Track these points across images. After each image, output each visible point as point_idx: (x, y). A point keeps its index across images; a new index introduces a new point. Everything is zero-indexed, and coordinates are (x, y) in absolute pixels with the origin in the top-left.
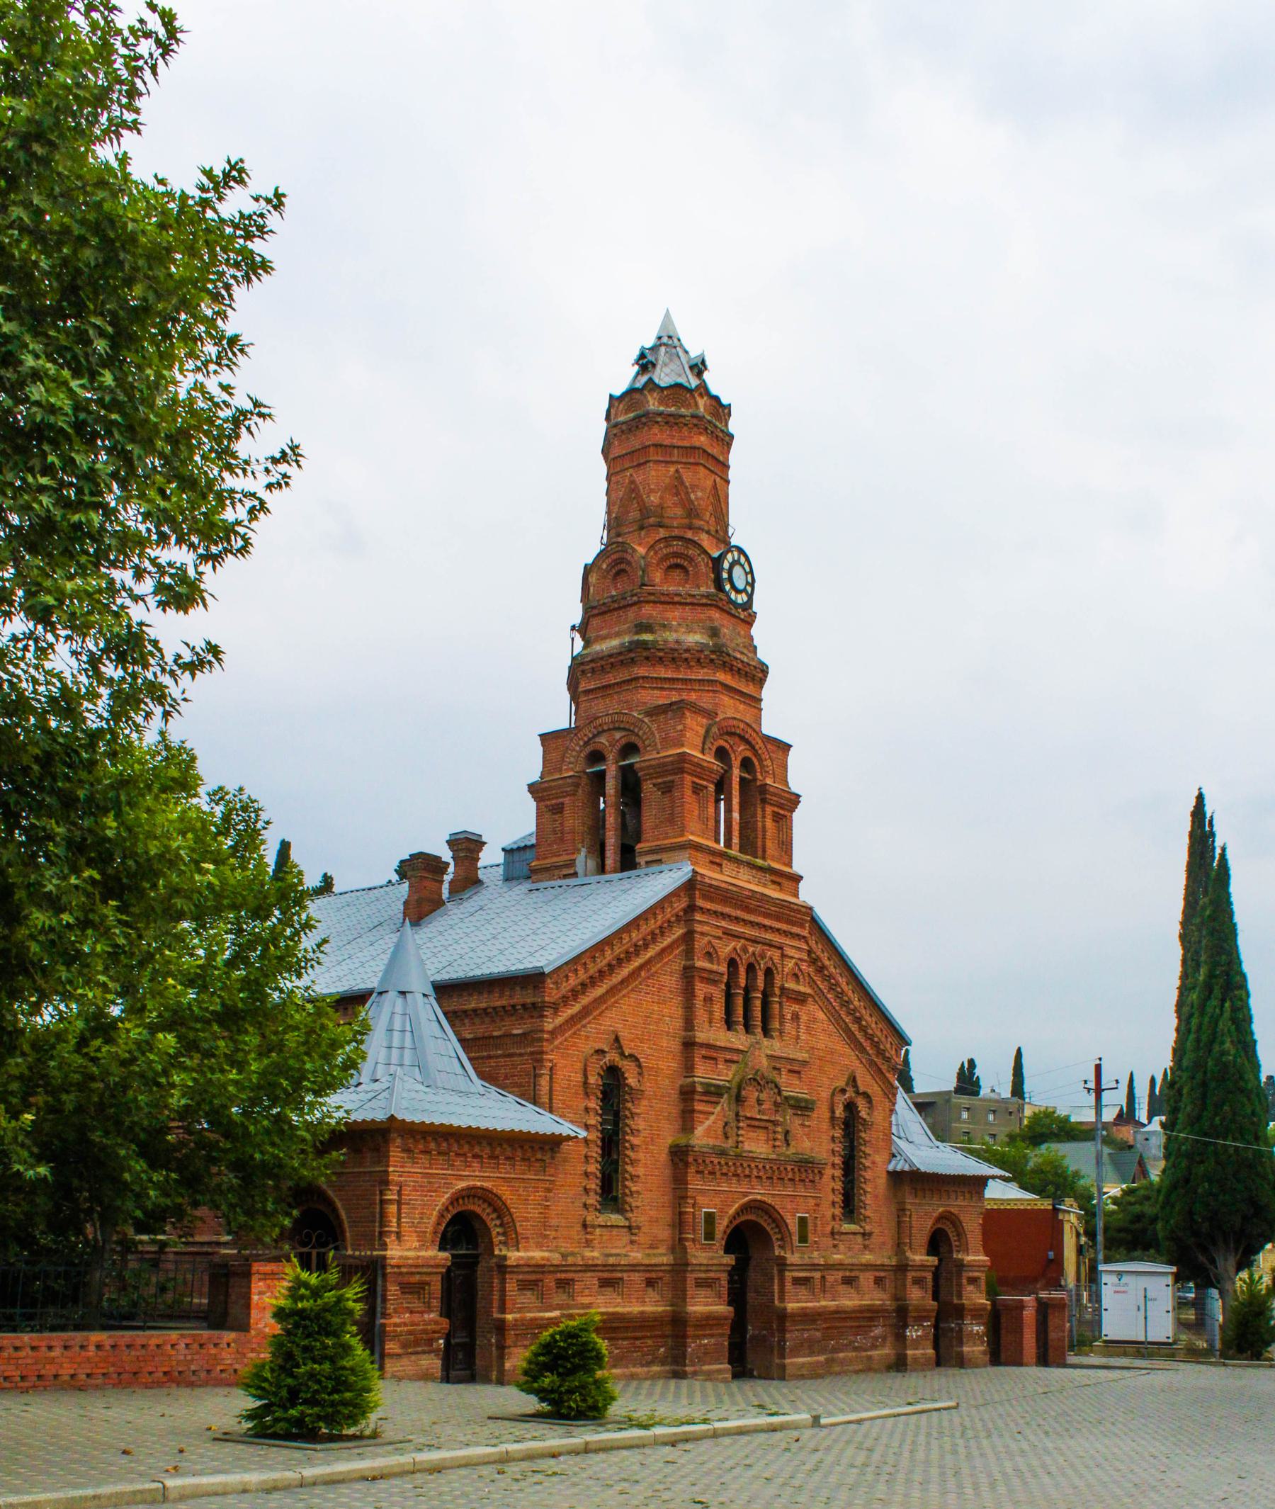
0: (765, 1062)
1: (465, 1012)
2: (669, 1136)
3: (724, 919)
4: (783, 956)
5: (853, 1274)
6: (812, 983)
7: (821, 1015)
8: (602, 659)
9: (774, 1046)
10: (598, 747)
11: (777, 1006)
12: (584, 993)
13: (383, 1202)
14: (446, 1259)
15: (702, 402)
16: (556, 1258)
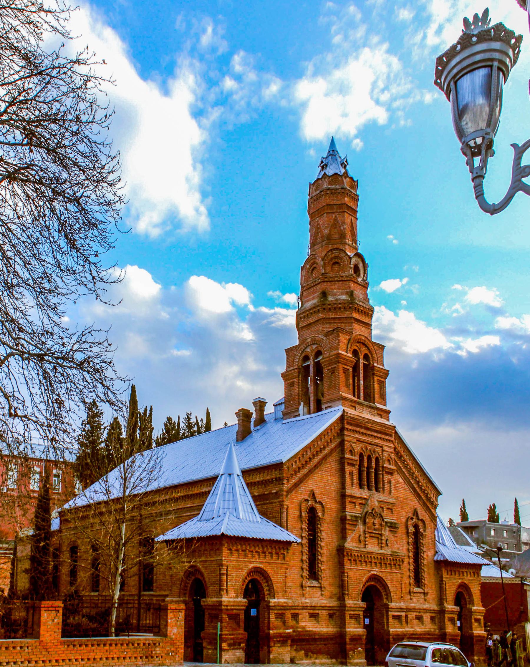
0: (376, 503)
1: (255, 483)
2: (335, 543)
3: (357, 433)
4: (383, 451)
5: (420, 614)
6: (396, 464)
7: (401, 480)
8: (307, 311)
9: (381, 496)
11: (381, 476)
12: (299, 472)
13: (221, 574)
14: (246, 602)
15: (346, 181)
16: (290, 602)
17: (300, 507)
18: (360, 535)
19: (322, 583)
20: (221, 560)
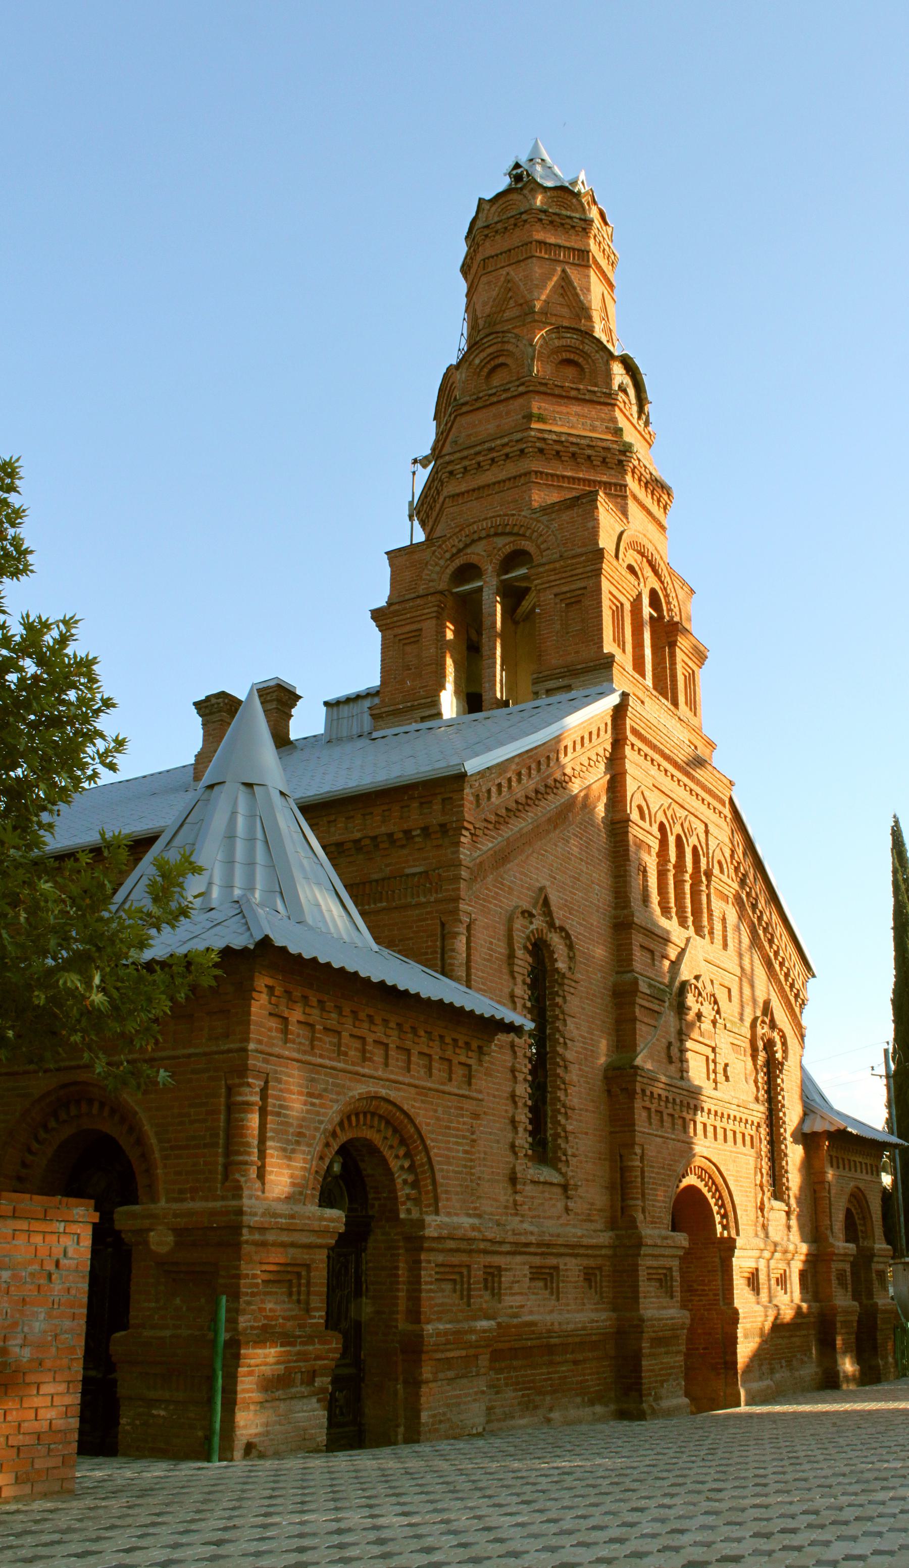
10: (474, 559)
17: (510, 930)
18: (670, 1044)
19: (570, 1174)
20: (245, 1050)
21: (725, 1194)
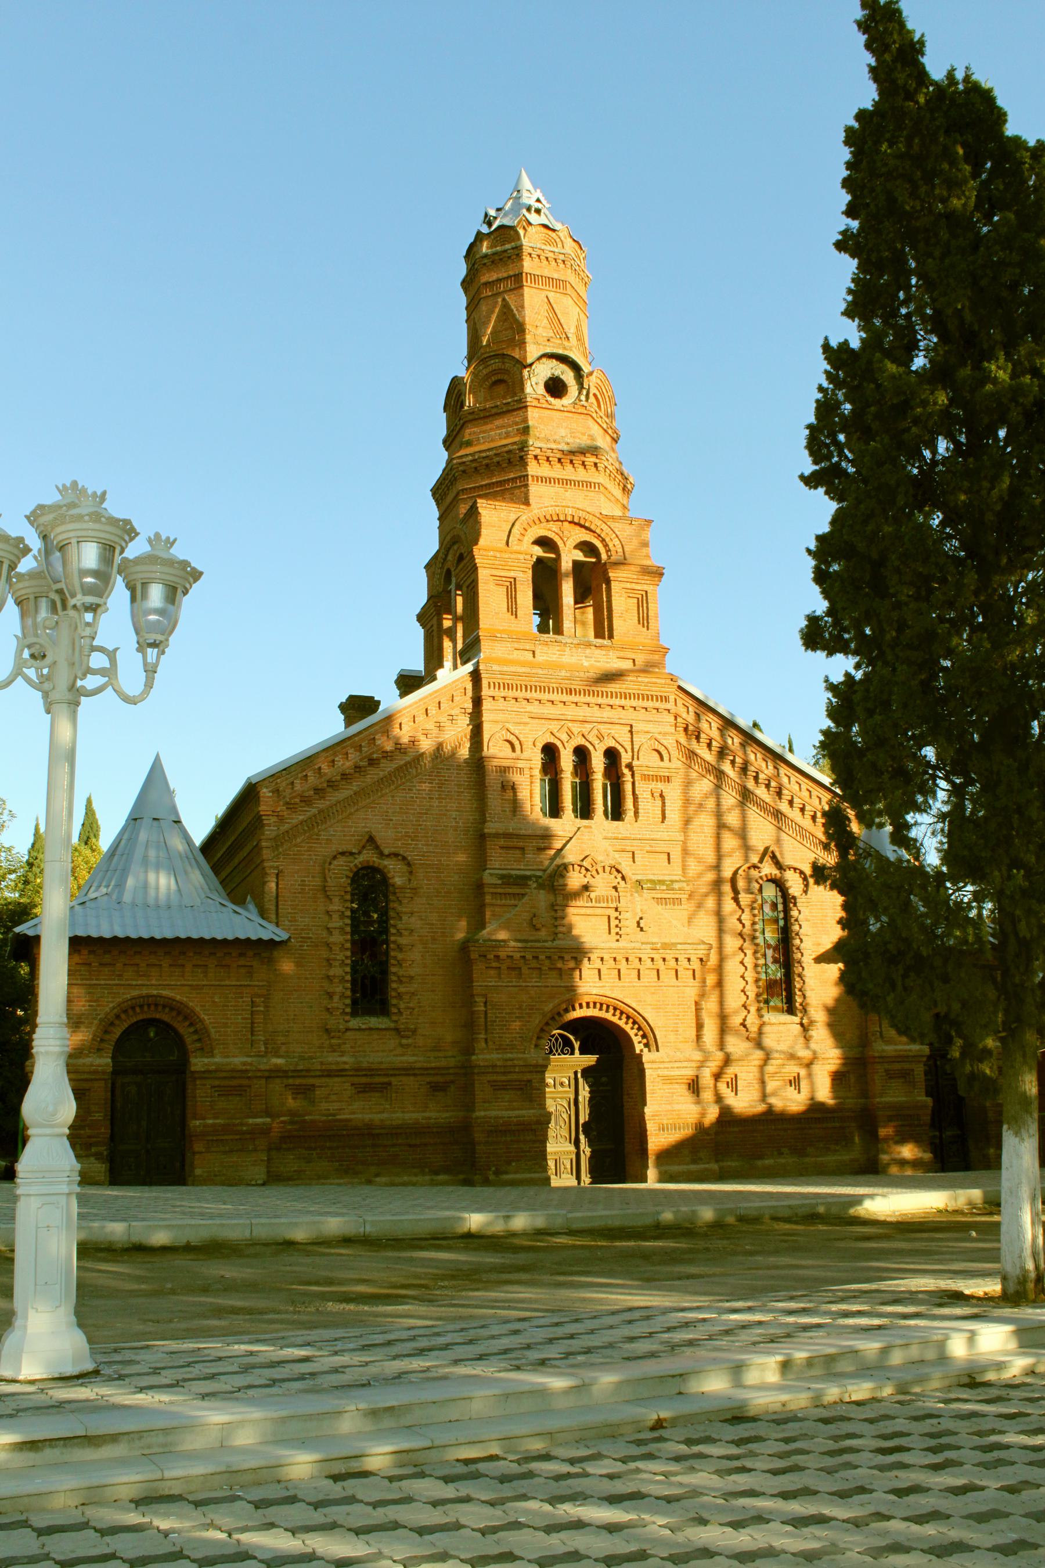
14: (107, 1065)
21: (644, 1024)
